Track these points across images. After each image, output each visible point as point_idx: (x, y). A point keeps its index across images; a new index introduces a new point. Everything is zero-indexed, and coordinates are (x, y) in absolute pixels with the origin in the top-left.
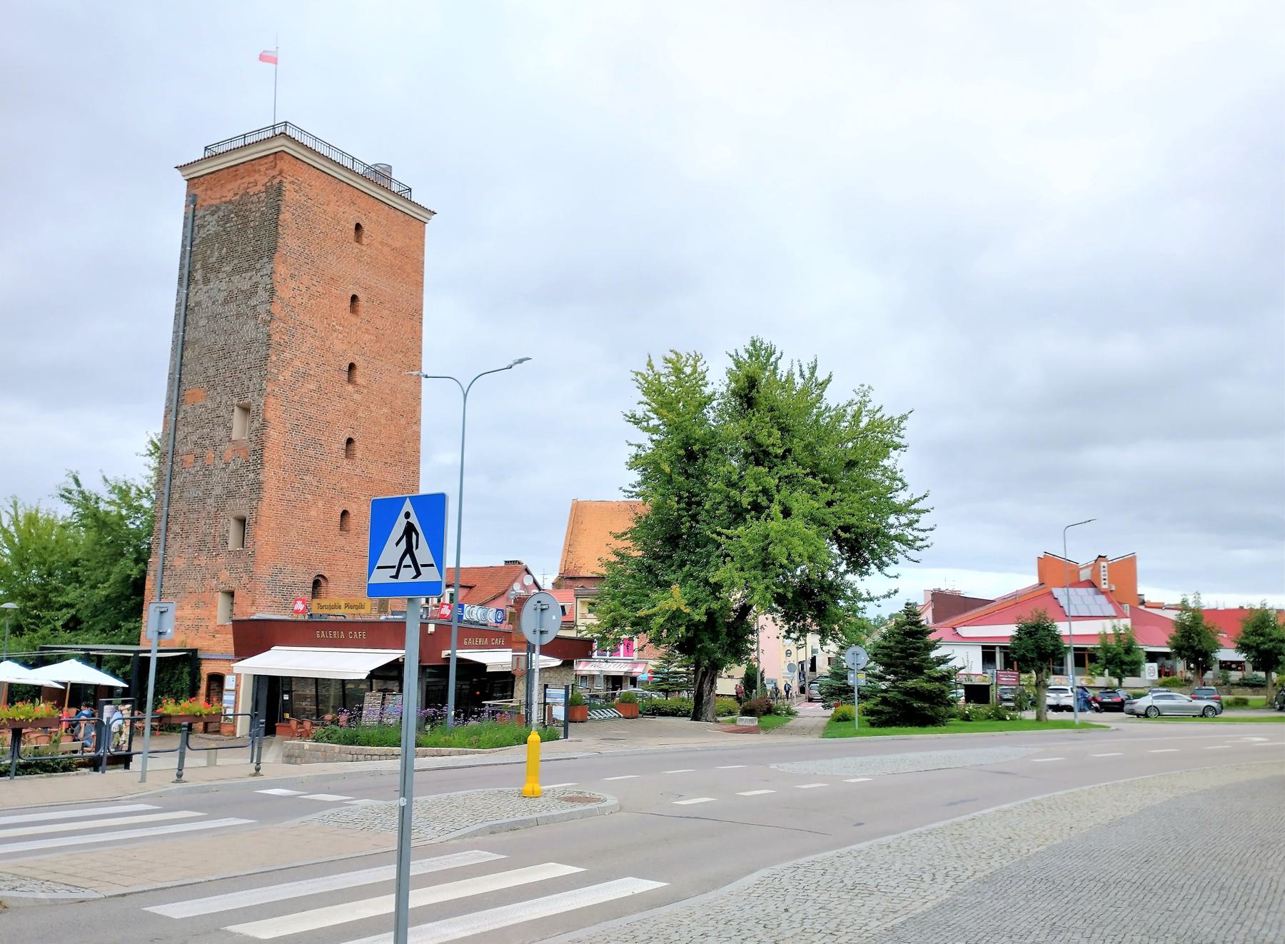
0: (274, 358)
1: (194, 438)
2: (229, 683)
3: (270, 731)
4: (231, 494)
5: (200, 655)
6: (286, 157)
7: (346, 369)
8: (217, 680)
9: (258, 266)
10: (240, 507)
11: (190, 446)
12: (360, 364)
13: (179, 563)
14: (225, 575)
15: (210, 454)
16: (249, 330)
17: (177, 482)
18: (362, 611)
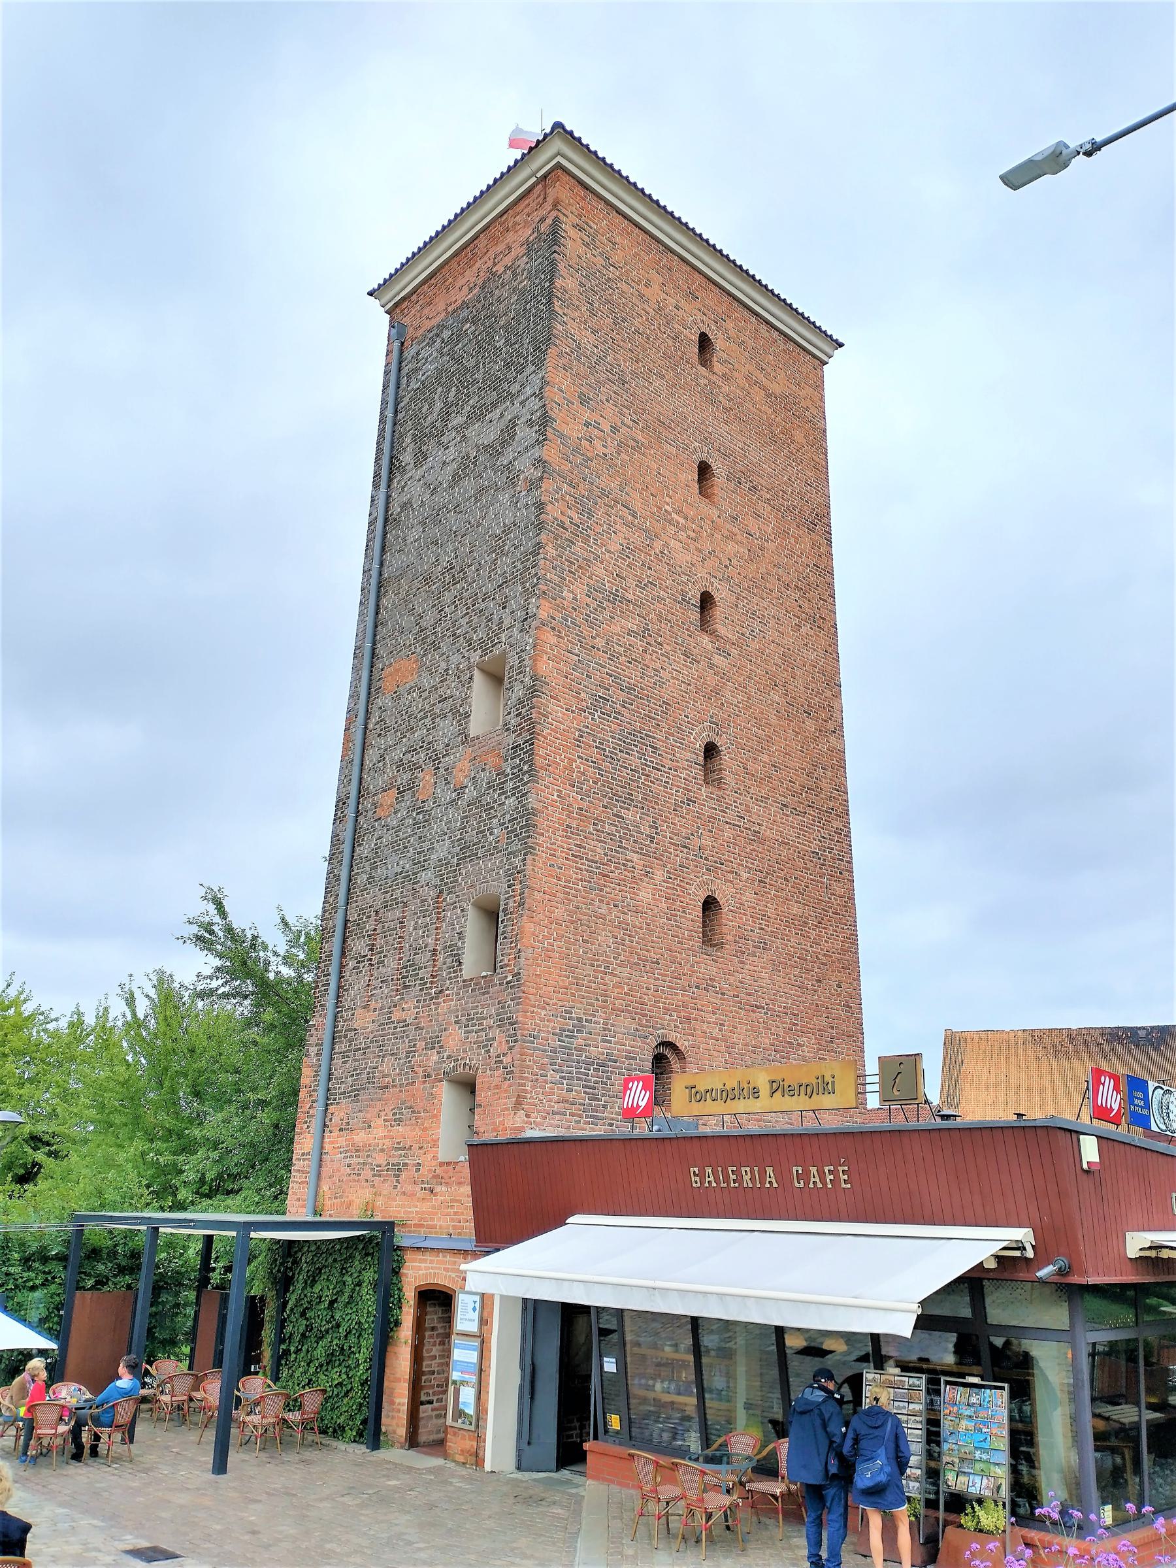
0: (551, 550)
1: (397, 754)
2: (465, 1318)
3: (570, 1455)
4: (467, 853)
5: (402, 1238)
6: (565, 178)
7: (696, 601)
8: (437, 1300)
9: (515, 388)
10: (487, 877)
11: (390, 772)
12: (721, 595)
13: (363, 1021)
14: (454, 1039)
15: (427, 778)
16: (503, 510)
17: (364, 850)
18: (827, 1101)
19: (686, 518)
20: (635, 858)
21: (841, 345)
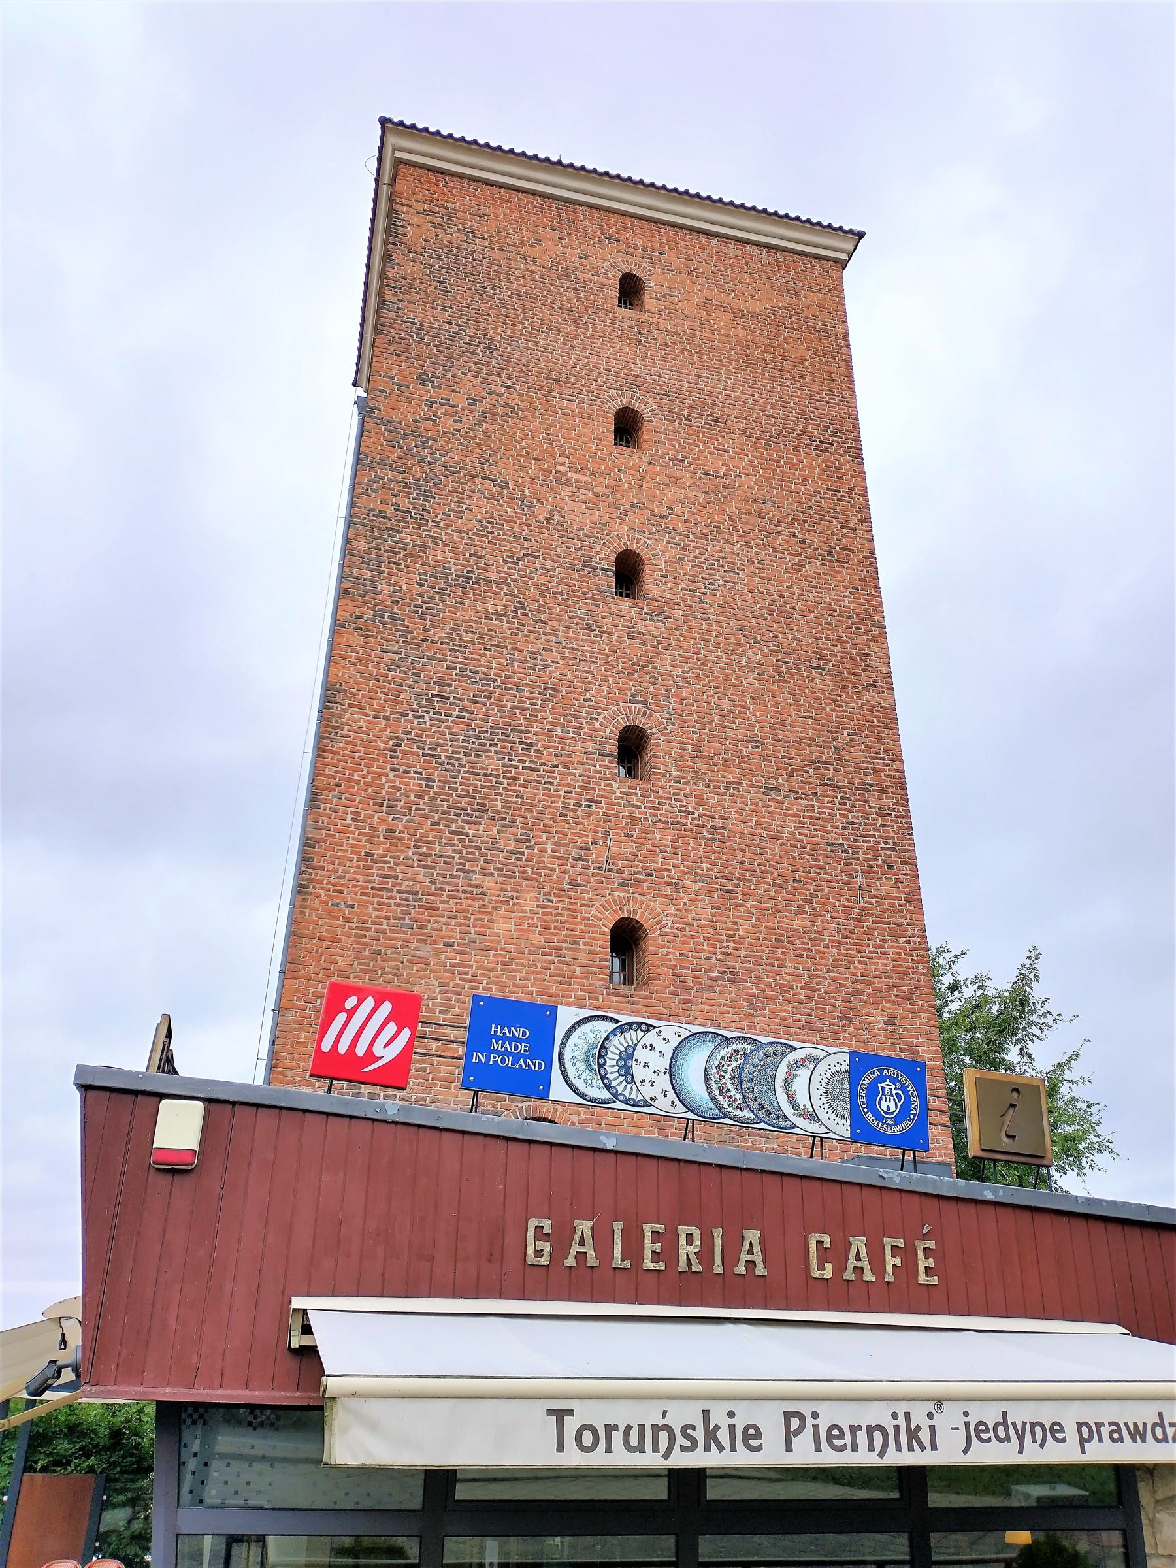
19: (593, 474)
20: (487, 882)
21: (861, 235)
